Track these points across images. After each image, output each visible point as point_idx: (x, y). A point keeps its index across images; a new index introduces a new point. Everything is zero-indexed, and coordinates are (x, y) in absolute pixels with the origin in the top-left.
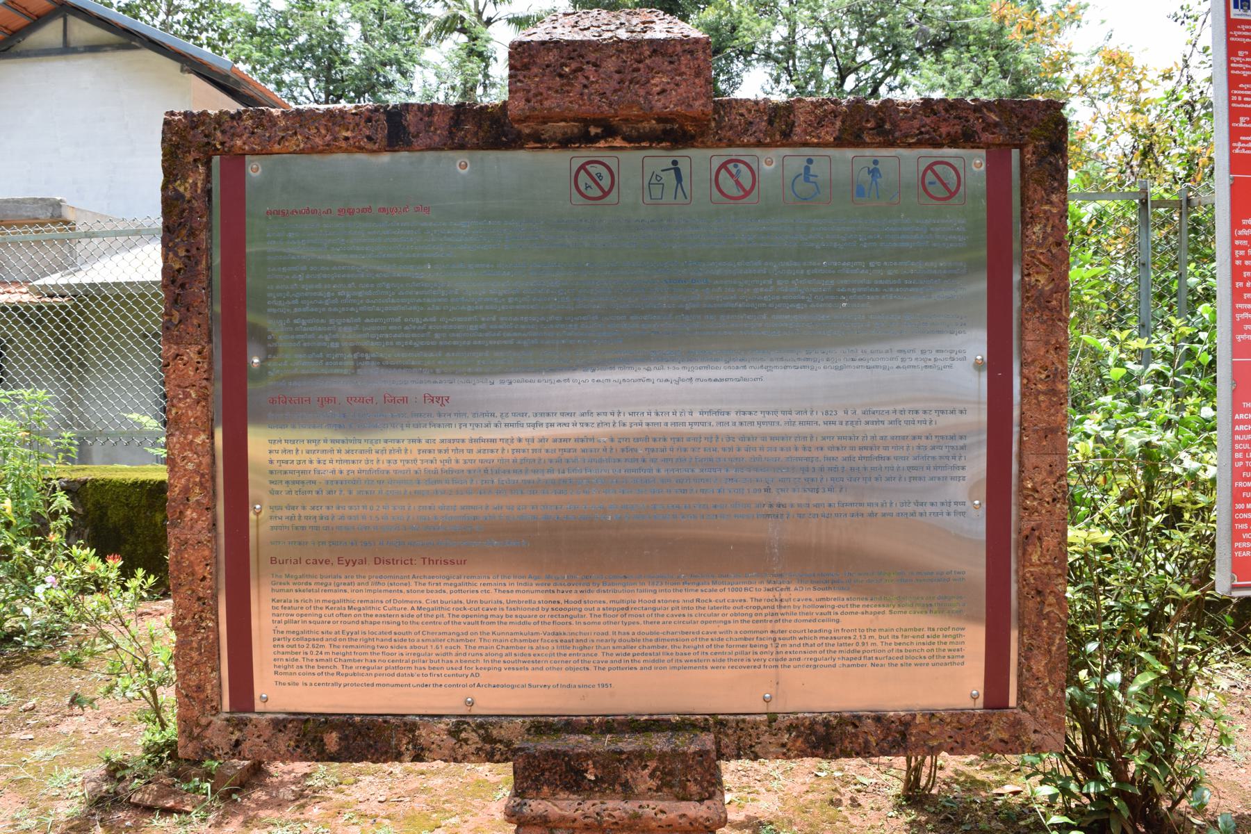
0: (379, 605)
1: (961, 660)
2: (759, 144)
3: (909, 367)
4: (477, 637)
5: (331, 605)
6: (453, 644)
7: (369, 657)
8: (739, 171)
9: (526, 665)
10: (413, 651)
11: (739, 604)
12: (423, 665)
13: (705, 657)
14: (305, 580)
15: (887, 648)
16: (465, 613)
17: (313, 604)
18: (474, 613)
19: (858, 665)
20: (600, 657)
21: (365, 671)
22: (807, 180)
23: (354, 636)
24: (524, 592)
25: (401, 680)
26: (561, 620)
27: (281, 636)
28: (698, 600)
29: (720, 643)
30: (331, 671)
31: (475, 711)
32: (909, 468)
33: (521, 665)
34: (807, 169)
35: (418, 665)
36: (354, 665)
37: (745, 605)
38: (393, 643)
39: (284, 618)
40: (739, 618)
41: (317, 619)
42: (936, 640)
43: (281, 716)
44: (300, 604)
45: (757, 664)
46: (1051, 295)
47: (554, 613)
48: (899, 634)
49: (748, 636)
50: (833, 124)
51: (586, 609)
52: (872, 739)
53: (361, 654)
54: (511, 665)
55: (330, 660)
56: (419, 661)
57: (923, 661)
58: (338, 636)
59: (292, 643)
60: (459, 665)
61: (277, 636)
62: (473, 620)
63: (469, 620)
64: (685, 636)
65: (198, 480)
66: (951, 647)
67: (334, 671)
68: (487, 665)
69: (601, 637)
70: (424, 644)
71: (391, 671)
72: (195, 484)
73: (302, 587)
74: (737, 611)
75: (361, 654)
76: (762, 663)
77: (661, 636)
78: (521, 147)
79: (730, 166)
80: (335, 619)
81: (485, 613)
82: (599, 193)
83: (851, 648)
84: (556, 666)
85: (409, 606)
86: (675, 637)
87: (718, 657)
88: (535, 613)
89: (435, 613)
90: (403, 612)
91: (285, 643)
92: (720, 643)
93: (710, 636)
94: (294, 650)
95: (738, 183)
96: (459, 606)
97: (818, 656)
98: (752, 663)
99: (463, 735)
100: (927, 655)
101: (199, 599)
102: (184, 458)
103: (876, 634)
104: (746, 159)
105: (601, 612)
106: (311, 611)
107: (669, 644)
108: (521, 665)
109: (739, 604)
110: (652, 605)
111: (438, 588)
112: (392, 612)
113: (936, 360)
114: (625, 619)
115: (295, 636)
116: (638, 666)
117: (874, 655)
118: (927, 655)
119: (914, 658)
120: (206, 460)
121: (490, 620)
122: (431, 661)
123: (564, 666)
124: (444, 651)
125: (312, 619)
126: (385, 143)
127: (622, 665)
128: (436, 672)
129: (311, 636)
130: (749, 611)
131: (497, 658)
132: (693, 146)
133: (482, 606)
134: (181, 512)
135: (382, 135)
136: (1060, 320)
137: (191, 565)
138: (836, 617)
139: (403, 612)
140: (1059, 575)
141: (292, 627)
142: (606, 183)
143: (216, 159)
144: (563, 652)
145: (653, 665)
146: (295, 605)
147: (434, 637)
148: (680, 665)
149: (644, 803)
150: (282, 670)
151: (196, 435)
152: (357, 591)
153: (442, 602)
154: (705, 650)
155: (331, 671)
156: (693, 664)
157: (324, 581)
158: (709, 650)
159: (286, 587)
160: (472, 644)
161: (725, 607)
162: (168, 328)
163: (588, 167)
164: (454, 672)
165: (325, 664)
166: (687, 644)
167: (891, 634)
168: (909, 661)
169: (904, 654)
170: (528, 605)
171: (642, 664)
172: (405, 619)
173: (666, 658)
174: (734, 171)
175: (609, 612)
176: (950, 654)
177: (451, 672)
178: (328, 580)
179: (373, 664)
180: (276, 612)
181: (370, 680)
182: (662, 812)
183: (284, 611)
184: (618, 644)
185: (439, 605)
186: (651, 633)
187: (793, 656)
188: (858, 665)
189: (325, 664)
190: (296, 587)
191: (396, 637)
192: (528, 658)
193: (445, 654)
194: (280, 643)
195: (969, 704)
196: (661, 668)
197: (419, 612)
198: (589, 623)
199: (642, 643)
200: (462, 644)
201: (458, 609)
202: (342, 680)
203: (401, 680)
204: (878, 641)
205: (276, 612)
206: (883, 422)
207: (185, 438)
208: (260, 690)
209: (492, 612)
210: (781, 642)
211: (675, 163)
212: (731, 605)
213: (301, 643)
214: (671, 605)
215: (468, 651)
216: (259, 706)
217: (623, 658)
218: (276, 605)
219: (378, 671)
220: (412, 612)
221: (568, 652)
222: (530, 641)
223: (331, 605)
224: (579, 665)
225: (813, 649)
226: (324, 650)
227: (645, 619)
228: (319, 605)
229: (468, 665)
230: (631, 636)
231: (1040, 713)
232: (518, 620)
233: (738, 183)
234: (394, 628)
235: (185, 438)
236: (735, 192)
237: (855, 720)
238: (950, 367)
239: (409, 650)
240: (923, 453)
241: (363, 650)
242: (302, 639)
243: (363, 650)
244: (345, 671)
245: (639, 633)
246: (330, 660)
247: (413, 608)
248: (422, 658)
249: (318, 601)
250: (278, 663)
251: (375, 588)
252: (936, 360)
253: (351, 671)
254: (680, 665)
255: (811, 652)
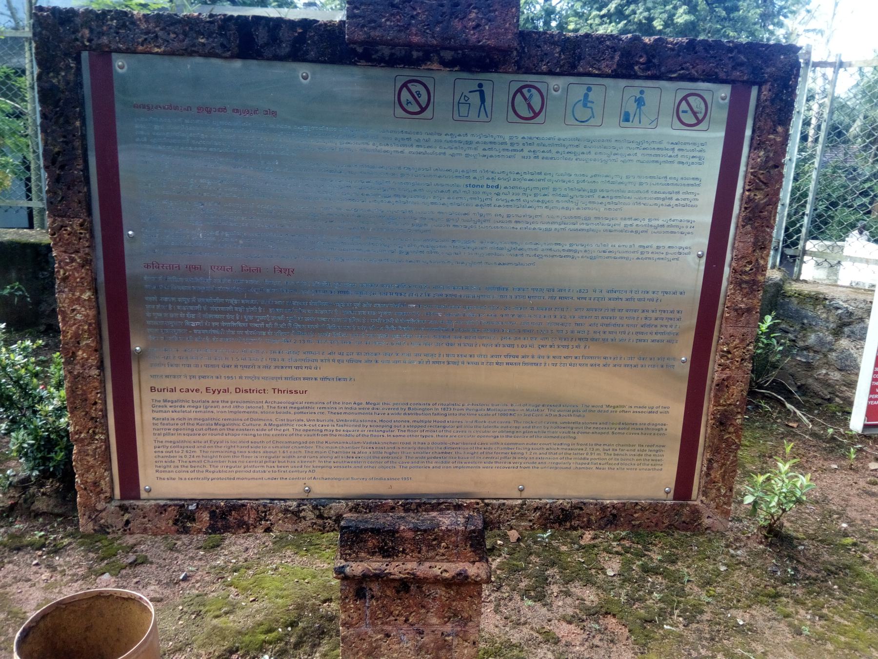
0: (239, 422)
1: (660, 467)
2: (551, 73)
3: (646, 258)
4: (314, 445)
5: (201, 422)
6: (296, 450)
7: (231, 459)
8: (531, 96)
9: (350, 465)
10: (265, 455)
11: (504, 425)
12: (272, 465)
13: (479, 460)
14: (179, 404)
15: (608, 457)
16: (305, 428)
17: (186, 422)
18: (312, 428)
19: (587, 468)
20: (404, 459)
21: (228, 469)
22: (585, 105)
23: (219, 445)
24: (349, 414)
25: (256, 475)
26: (376, 433)
27: (161, 445)
28: (476, 421)
29: (490, 451)
30: (201, 469)
31: (311, 496)
32: (637, 333)
33: (347, 464)
34: (586, 96)
35: (269, 464)
36: (219, 465)
37: (509, 425)
38: (250, 449)
39: (163, 432)
40: (504, 434)
41: (189, 432)
42: (644, 453)
43: (162, 503)
44: (176, 422)
45: (515, 465)
46: (764, 208)
47: (372, 429)
48: (618, 448)
49: (510, 447)
50: (612, 58)
51: (395, 426)
52: (593, 518)
53: (224, 457)
54: (338, 464)
55: (201, 461)
56: (270, 462)
57: (633, 467)
58: (207, 445)
59: (169, 449)
60: (300, 464)
61: (157, 444)
62: (311, 433)
63: (309, 433)
64: (465, 446)
65: (86, 327)
66: (654, 458)
67: (204, 469)
68: (321, 464)
69: (405, 446)
70: (274, 450)
71: (249, 469)
72: (84, 331)
73: (178, 409)
74: (503, 429)
75: (224, 457)
76: (519, 465)
77: (449, 446)
78: (354, 64)
79: (525, 91)
80: (205, 432)
81: (321, 428)
82: (418, 109)
83: (583, 456)
84: (372, 465)
85: (262, 423)
86: (458, 446)
87: (488, 460)
88: (357, 428)
89: (282, 428)
90: (258, 427)
91: (164, 450)
92: (490, 451)
93: (483, 446)
94: (171, 454)
95: (530, 107)
96: (301, 423)
97: (560, 461)
98: (512, 465)
99: (302, 514)
100: (636, 463)
101: (92, 418)
102: (73, 310)
103: (601, 448)
104: (538, 85)
105: (406, 429)
106: (186, 427)
107: (453, 451)
108: (347, 464)
109: (504, 425)
110: (443, 424)
111: (285, 410)
112: (250, 427)
113: (667, 253)
114: (423, 434)
115: (172, 444)
116: (431, 465)
117: (599, 462)
118: (636, 463)
119: (626, 464)
120: (92, 313)
121: (324, 433)
122: (279, 462)
123: (378, 465)
124: (289, 454)
125: (186, 432)
126: (236, 50)
127: (419, 465)
128: (283, 469)
129: (186, 444)
130: (512, 430)
131: (329, 460)
132: (496, 72)
133: (318, 423)
134: (73, 353)
135: (234, 45)
136: (768, 227)
137: (84, 393)
138: (573, 435)
139: (258, 427)
140: (738, 413)
141: (168, 438)
142: (423, 99)
143: (85, 55)
144: (377, 455)
145: (442, 465)
146: (172, 422)
147: (282, 445)
148: (461, 465)
149: (433, 564)
150: (162, 469)
151: (82, 292)
152: (222, 412)
153: (288, 420)
154: (479, 455)
155: (201, 469)
156: (470, 465)
157: (195, 404)
158: (482, 456)
159: (164, 409)
160: (310, 450)
161: (495, 427)
162: (51, 203)
163: (409, 85)
164: (297, 469)
165: (196, 464)
166: (466, 451)
167: (611, 448)
168: (623, 467)
169: (620, 461)
170: (352, 423)
171: (434, 465)
172: (259, 432)
173: (451, 460)
174: (527, 95)
175: (411, 429)
176: (653, 463)
177: (294, 469)
178: (198, 404)
179: (234, 464)
180: (156, 427)
181: (233, 475)
182: (446, 571)
183: (162, 427)
184: (417, 450)
185: (286, 422)
186: (442, 443)
187: (541, 461)
188: (587, 468)
189: (196, 464)
190: (173, 409)
191: (252, 445)
192: (351, 460)
193: (289, 457)
194: (160, 450)
195: (662, 495)
196: (447, 467)
197: (270, 428)
198: (397, 436)
199: (434, 450)
200: (303, 450)
201: (300, 425)
202: (211, 475)
203: (256, 475)
204: (602, 453)
205: (156, 427)
206: (621, 299)
207: (73, 295)
208: (144, 484)
209: (326, 428)
210: (533, 451)
211: (480, 85)
212: (499, 425)
213: (177, 449)
214: (456, 424)
215: (307, 455)
216: (143, 495)
217: (420, 460)
218: (156, 422)
219: (239, 469)
220: (265, 427)
221: (381, 455)
222: (353, 448)
223: (201, 422)
224: (389, 465)
225: (556, 456)
226: (195, 455)
227: (438, 433)
228: (191, 422)
229: (307, 464)
230: (426, 446)
231: (713, 505)
232: (345, 433)
233: (530, 107)
234: (251, 438)
235: (73, 295)
236: (526, 113)
237: (580, 506)
238: (677, 259)
239: (262, 454)
240: (648, 322)
241: (226, 454)
242: (178, 447)
243: (226, 454)
244: (212, 469)
245: (433, 443)
246: (201, 461)
247: (265, 425)
248: (272, 459)
249: (191, 419)
250: (158, 464)
251: (236, 410)
252: (667, 253)
253: (217, 469)
254: (461, 465)
255: (554, 458)
